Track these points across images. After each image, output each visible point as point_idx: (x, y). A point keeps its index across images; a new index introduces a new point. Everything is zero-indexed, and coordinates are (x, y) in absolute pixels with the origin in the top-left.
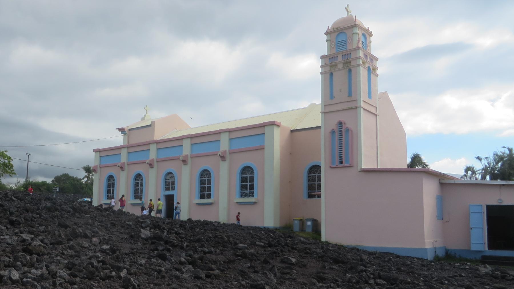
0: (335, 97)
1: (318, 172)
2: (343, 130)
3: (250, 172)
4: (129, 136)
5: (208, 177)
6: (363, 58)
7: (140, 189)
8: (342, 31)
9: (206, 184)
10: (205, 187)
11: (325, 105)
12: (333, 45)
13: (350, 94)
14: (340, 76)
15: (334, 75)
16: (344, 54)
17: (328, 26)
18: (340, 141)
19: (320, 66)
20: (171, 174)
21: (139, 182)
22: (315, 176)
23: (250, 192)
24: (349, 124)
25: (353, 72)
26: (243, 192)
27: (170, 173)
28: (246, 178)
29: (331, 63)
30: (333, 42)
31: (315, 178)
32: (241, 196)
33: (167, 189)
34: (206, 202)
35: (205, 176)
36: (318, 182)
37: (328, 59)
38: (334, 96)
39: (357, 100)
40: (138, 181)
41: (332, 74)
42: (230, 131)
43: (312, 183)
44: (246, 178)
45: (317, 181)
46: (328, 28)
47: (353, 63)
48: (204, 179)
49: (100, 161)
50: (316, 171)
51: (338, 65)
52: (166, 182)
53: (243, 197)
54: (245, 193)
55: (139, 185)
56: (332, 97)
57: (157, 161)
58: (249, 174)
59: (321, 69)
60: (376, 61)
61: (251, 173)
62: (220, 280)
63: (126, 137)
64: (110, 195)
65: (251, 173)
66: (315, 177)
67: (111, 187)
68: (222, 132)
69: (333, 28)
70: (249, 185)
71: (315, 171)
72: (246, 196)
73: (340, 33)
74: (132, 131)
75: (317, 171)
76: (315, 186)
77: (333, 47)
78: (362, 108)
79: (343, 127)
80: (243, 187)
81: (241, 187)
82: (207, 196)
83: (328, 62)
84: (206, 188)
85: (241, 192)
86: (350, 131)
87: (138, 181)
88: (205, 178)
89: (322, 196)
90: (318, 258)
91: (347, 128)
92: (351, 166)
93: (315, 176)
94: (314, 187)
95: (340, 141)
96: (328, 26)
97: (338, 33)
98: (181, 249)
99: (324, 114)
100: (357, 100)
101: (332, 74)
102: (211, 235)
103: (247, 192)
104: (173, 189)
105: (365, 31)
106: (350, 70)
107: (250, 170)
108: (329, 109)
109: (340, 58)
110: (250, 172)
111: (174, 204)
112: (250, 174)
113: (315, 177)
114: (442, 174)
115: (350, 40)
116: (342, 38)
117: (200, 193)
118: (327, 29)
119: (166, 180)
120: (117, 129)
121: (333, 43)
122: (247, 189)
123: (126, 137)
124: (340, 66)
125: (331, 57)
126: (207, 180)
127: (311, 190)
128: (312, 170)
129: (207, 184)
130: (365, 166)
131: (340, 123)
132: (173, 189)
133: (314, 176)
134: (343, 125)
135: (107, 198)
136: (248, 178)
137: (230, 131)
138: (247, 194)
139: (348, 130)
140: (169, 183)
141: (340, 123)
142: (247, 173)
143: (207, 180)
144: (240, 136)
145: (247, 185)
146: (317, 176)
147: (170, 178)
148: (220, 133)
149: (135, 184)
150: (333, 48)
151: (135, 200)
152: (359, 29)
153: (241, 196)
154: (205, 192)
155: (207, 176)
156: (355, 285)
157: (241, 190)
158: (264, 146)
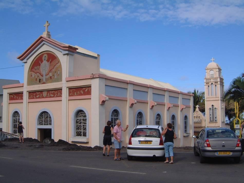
2: (214, 108)
27: (45, 112)
131: (213, 105)
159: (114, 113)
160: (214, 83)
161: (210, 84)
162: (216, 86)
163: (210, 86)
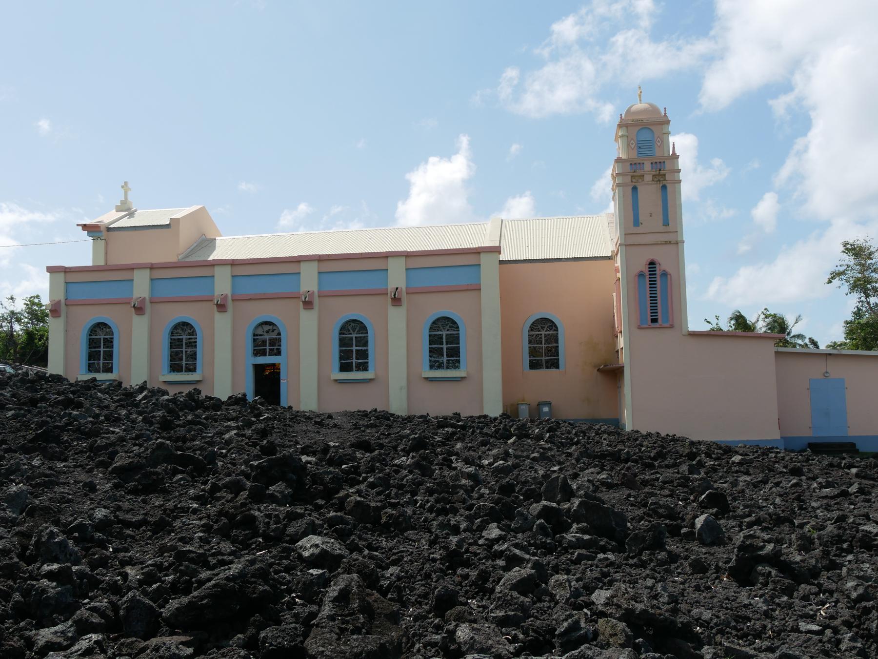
0: (642, 224)
1: (545, 329)
2: (658, 272)
3: (448, 327)
4: (106, 243)
7: (186, 352)
8: (648, 127)
9: (354, 345)
10: (352, 351)
12: (632, 144)
13: (666, 223)
14: (648, 192)
15: (638, 190)
16: (655, 161)
17: (621, 115)
20: (268, 326)
21: (182, 339)
22: (541, 335)
24: (664, 264)
25: (669, 189)
26: (435, 361)
28: (441, 337)
29: (634, 172)
30: (632, 139)
31: (541, 338)
32: (431, 367)
33: (258, 352)
34: (362, 378)
35: (351, 331)
36: (545, 344)
37: (628, 164)
38: (640, 221)
40: (181, 337)
41: (635, 189)
42: (407, 255)
43: (537, 345)
44: (441, 337)
45: (543, 343)
46: (621, 117)
47: (668, 177)
48: (347, 337)
49: (66, 291)
50: (542, 327)
51: (645, 176)
52: (255, 340)
53: (435, 369)
54: (438, 361)
55: (182, 345)
56: (637, 222)
57: (233, 300)
63: (102, 243)
64: (98, 364)
66: (540, 336)
67: (100, 347)
68: (390, 256)
71: (539, 327)
72: (440, 366)
73: (642, 128)
74: (111, 233)
75: (544, 327)
76: (541, 350)
77: (633, 146)
79: (657, 269)
80: (434, 352)
81: (430, 351)
82: (356, 367)
83: (628, 168)
85: (430, 361)
86: (669, 276)
87: (181, 337)
88: (351, 334)
89: (197, 353)
90: (700, 461)
92: (672, 327)
93: (541, 335)
94: (540, 352)
96: (621, 115)
97: (641, 127)
101: (635, 189)
104: (279, 353)
106: (664, 187)
109: (647, 167)
111: (282, 381)
112: (448, 330)
113: (540, 336)
115: (659, 142)
116: (645, 136)
117: (340, 361)
119: (254, 335)
120: (78, 225)
121: (632, 142)
122: (443, 355)
123: (102, 243)
124: (648, 178)
125: (633, 163)
126: (356, 337)
127: (534, 357)
128: (535, 326)
130: (692, 327)
132: (279, 353)
133: (538, 335)
134: (657, 266)
135: (89, 370)
136: (444, 337)
137: (408, 255)
138: (443, 363)
139: (665, 274)
140: (264, 342)
141: (652, 264)
143: (356, 337)
145: (442, 348)
146: (543, 335)
147: (265, 333)
148: (387, 257)
149: (171, 343)
151: (172, 373)
153: (431, 367)
154: (352, 360)
155: (354, 331)
156: (520, 509)
157: (430, 357)
158: (480, 285)
159: (104, 329)
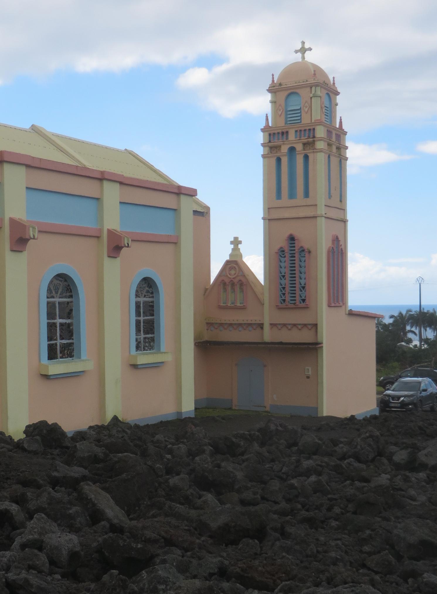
5: (60, 298)
6: (326, 138)
11: (268, 208)
18: (291, 276)
19: (262, 144)
23: (145, 338)
35: (54, 292)
39: (316, 205)
46: (273, 81)
58: (143, 295)
59: (263, 134)
60: (346, 161)
61: (146, 294)
62: (99, 441)
65: (146, 294)
69: (279, 82)
70: (144, 322)
77: (280, 113)
78: (324, 217)
79: (296, 245)
84: (56, 327)
91: (302, 247)
95: (291, 276)
98: (26, 225)
99: (268, 220)
100: (316, 205)
102: (71, 511)
103: (140, 338)
105: (328, 127)
107: (144, 287)
108: (276, 214)
110: (145, 291)
114: (419, 377)
118: (271, 82)
129: (60, 318)
141: (292, 238)
142: (141, 294)
144: (123, 202)
150: (280, 116)
152: (323, 89)
154: (56, 340)
155: (57, 293)
160: (299, 147)
161: (285, 149)
162: (306, 157)
163: (285, 161)
